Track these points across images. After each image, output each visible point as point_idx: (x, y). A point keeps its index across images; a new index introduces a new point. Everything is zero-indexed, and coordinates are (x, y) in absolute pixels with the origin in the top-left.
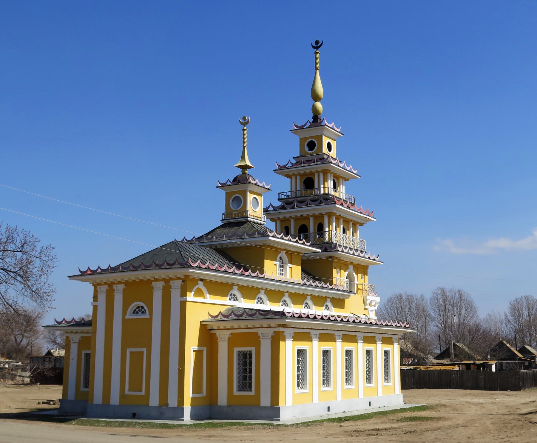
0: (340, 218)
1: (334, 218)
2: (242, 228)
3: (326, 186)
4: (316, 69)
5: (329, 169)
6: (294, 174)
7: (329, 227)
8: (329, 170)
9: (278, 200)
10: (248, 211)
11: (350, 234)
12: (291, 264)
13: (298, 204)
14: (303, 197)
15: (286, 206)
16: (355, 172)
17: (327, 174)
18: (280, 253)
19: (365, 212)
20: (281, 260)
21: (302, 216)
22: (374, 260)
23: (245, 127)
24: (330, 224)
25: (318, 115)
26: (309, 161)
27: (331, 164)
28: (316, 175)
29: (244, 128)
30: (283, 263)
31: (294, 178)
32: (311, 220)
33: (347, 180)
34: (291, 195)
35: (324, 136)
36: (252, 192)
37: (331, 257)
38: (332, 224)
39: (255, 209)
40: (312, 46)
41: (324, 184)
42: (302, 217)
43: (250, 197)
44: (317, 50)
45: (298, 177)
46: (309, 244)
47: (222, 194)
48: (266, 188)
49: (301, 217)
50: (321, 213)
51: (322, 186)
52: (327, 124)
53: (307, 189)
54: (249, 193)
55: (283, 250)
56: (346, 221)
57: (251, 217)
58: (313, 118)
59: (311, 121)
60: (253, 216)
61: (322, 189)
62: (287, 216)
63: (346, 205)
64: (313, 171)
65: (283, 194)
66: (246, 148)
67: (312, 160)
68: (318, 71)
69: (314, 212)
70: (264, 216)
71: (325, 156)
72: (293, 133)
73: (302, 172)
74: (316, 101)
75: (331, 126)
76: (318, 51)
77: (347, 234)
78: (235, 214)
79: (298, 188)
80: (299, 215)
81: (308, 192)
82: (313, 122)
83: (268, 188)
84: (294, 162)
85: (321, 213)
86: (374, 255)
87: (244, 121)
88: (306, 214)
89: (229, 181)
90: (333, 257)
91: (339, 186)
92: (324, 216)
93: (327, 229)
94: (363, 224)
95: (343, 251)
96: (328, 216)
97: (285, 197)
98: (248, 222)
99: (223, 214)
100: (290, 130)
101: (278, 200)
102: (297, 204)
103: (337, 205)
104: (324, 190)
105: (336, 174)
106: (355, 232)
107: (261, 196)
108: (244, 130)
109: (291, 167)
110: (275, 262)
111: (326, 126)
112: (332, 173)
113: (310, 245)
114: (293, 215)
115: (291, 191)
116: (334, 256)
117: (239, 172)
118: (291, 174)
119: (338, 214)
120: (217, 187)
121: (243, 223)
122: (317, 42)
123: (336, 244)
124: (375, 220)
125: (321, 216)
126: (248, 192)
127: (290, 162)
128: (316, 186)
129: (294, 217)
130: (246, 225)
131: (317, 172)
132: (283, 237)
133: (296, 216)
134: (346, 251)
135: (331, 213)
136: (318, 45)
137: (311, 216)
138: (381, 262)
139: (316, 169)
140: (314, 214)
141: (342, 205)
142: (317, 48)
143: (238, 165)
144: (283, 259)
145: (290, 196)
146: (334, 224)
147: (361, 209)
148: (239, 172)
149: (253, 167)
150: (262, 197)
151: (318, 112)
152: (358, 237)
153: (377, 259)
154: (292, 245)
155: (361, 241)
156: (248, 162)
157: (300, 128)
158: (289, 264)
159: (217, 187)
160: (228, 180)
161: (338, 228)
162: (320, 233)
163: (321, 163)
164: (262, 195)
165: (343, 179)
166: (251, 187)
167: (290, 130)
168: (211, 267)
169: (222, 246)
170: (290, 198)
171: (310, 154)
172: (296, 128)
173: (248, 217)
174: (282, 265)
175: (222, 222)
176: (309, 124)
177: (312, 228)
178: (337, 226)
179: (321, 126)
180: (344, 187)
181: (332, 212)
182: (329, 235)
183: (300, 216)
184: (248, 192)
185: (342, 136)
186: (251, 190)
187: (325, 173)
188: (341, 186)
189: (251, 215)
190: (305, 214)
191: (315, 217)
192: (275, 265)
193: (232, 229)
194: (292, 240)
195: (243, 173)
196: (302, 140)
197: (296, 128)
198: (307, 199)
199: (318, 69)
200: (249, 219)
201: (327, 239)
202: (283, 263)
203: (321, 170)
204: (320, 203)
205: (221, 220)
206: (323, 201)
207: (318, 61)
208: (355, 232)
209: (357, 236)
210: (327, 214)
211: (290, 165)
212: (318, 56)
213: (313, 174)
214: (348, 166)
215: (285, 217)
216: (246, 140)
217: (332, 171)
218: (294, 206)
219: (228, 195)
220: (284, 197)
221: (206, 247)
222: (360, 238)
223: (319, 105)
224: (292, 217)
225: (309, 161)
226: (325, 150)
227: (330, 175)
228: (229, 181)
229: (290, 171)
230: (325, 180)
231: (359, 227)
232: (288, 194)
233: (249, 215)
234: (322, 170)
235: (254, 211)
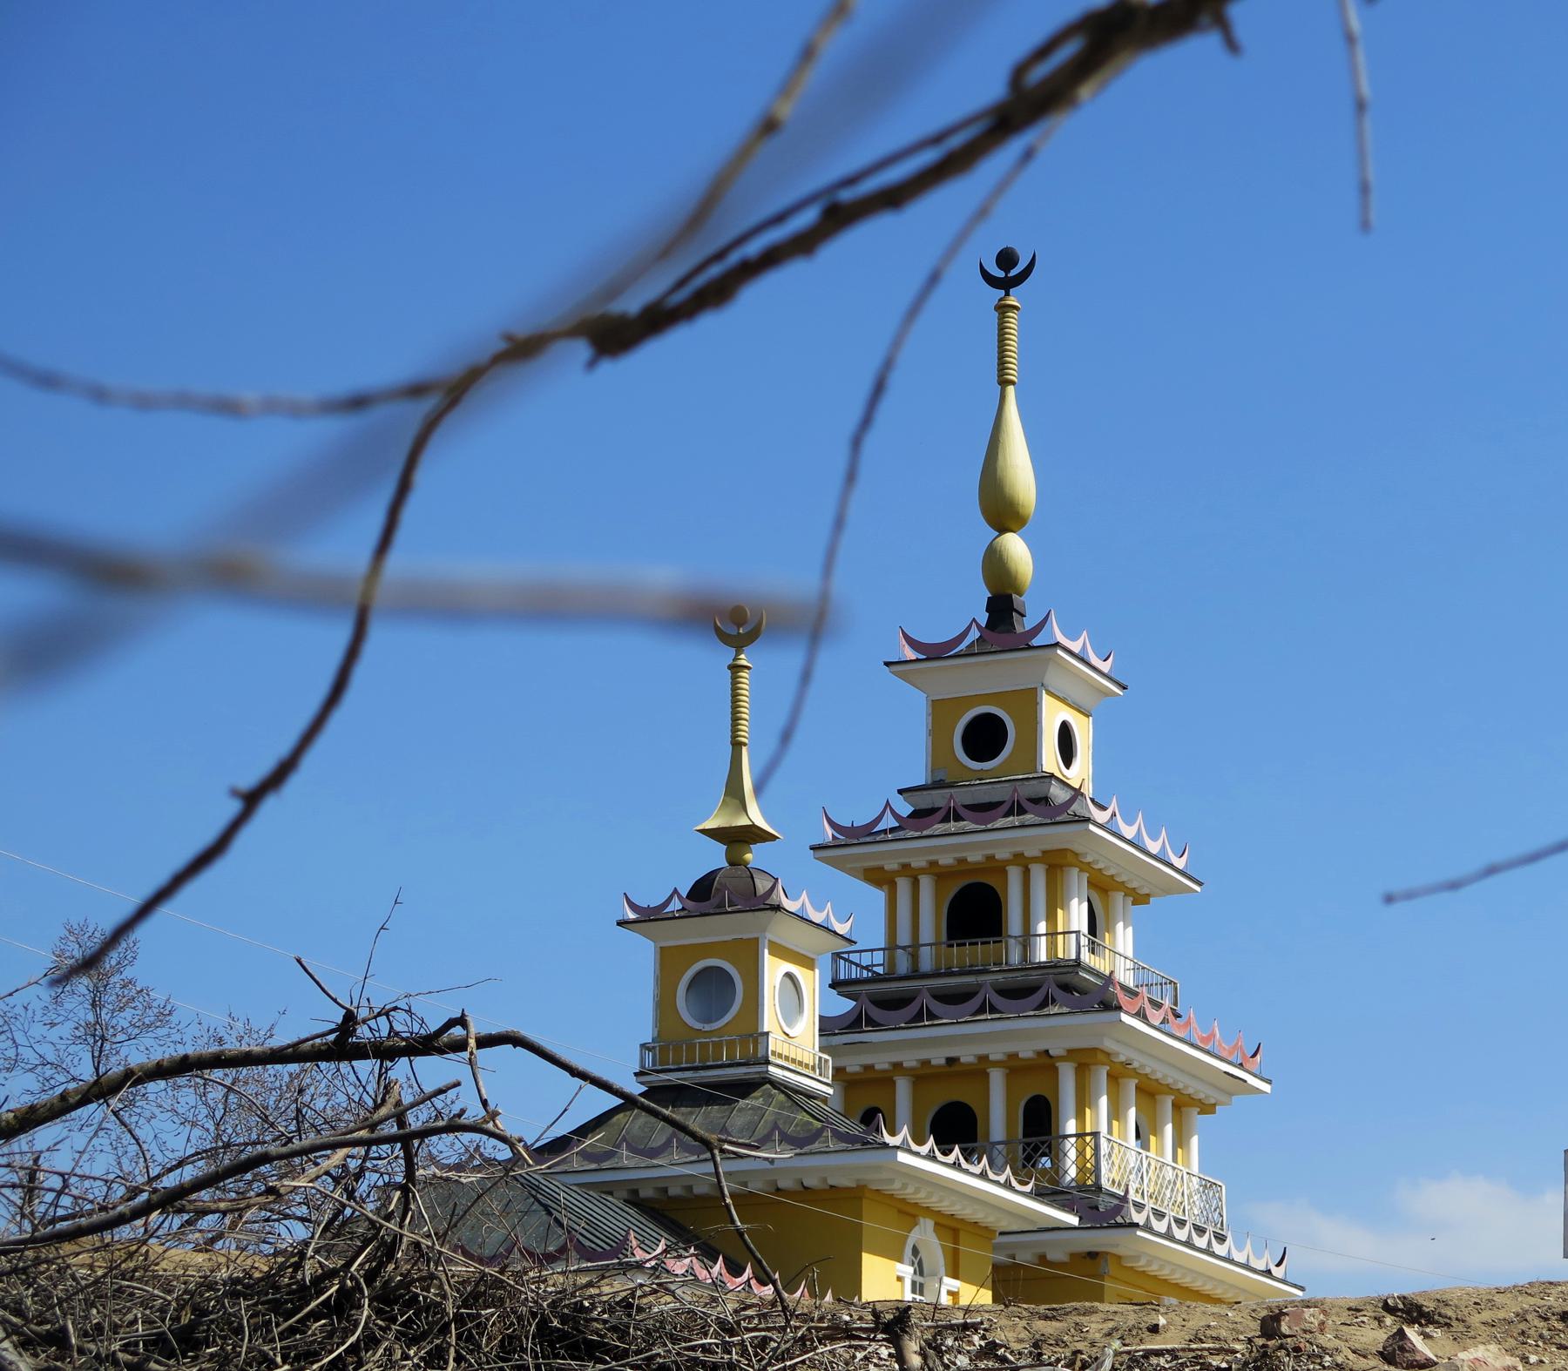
0: (1123, 1077)
1: (1103, 1072)
2: (740, 1110)
3: (1060, 929)
4: (1004, 383)
5: (1077, 848)
6: (906, 866)
7: (1080, 1116)
8: (1077, 854)
9: (830, 986)
10: (767, 1034)
11: (1161, 1152)
12: (955, 1276)
13: (937, 1007)
14: (952, 974)
15: (876, 1013)
16: (1180, 863)
17: (1062, 871)
18: (917, 1227)
19: (1231, 1053)
20: (916, 1257)
21: (951, 1061)
22: (1268, 1273)
23: (742, 656)
24: (1084, 1102)
25: (1014, 596)
26: (984, 809)
27: (1091, 827)
28: (1014, 874)
29: (736, 659)
30: (921, 1274)
31: (903, 885)
32: (997, 1079)
33: (1140, 899)
34: (891, 962)
35: (1050, 693)
36: (781, 952)
37: (1093, 1255)
38: (1094, 1105)
39: (789, 1024)
40: (985, 275)
41: (1051, 918)
42: (955, 1068)
43: (774, 970)
44: (1007, 294)
45: (926, 884)
46: (1028, 1188)
47: (641, 952)
48: (835, 933)
49: (948, 1069)
50: (1047, 1051)
51: (1042, 927)
52: (1061, 638)
53: (974, 940)
54: (770, 954)
55: (929, 1212)
56: (1149, 1092)
57: (779, 1062)
58: (987, 611)
59: (983, 618)
60: (787, 1058)
61: (1042, 943)
62: (882, 1062)
63: (1156, 1016)
64: (1002, 854)
65: (846, 956)
66: (744, 750)
67: (1000, 803)
68: (1011, 390)
69: (1011, 1047)
70: (826, 1061)
71: (1051, 790)
72: (903, 676)
73: (946, 860)
74: (1002, 530)
75: (1076, 647)
76: (1012, 301)
77: (1149, 1151)
78: (704, 1046)
79: (927, 933)
80: (938, 1057)
81: (974, 952)
82: (991, 625)
83: (841, 933)
84: (905, 809)
85: (1047, 1051)
86: (1267, 1255)
87: (739, 626)
88: (918, 1058)
89: (676, 897)
90: (1107, 1253)
91: (1110, 928)
92: (1057, 1064)
93: (1071, 1127)
94: (1214, 1105)
95: (1148, 1228)
96: (1074, 1065)
97: (865, 974)
98: (768, 1086)
99: (643, 1046)
100: (887, 664)
101: (830, 986)
102: (869, 1013)
103: (1125, 1018)
104: (1052, 946)
105: (1112, 876)
106: (1180, 1141)
107: (813, 970)
108: (735, 668)
109: (901, 834)
110: (898, 1265)
111: (1059, 652)
112: (1085, 867)
113: (1031, 1193)
114: (910, 1059)
115: (891, 947)
116: (1103, 1250)
117: (715, 857)
118: (891, 865)
119: (1122, 1058)
120: (620, 924)
121: (745, 1088)
122: (1006, 258)
123: (1124, 1199)
124: (1266, 1087)
125: (1046, 1064)
126: (766, 951)
127: (891, 808)
128: (1014, 924)
129: (912, 1069)
130: (757, 1098)
131: (1022, 861)
132: (934, 1151)
133: (926, 1063)
134: (1160, 1226)
135: (1094, 1051)
136: (1013, 273)
137: (997, 1064)
138: (1295, 1286)
139: (1018, 849)
140: (1013, 1056)
141: (1141, 1015)
142: (1006, 285)
143: (701, 827)
144: (923, 1254)
145: (880, 970)
146: (1103, 1101)
147: (1214, 1035)
148: (715, 857)
149: (774, 838)
150: (817, 971)
151: (1016, 578)
152: (1195, 1169)
153: (1278, 1272)
154: (962, 1190)
155: (1207, 1186)
156: (755, 815)
157: (933, 653)
158: (947, 1276)
159: (620, 924)
160: (675, 891)
161: (1115, 1123)
162: (1043, 1143)
163: (1038, 820)
164: (817, 963)
165: (1126, 895)
166: (780, 930)
167: (887, 664)
168: (700, 1274)
169: (665, 1190)
170: (877, 979)
171: (980, 775)
172: (910, 654)
173: (768, 1062)
174: (919, 1279)
175: (642, 1083)
176: (974, 634)
177: (999, 1119)
178: (1116, 1113)
179: (1031, 648)
180: (1130, 929)
181: (1100, 1047)
182: (1081, 1153)
183: (943, 1061)
184: (766, 951)
185: (1121, 693)
186: (778, 941)
187: (1057, 863)
188: (1120, 926)
189: (780, 1056)
190: (967, 1055)
191: (1015, 1068)
192: (900, 1279)
193: (691, 1113)
194: (991, 1175)
195: (732, 864)
196: (941, 710)
197: (910, 654)
198: (980, 986)
199: (1012, 383)
200: (771, 1068)
201: (1072, 1172)
202: (921, 1274)
203: (1011, 857)
204: (1044, 1004)
205: (636, 1074)
206: (1058, 994)
207: (1013, 345)
208: (1180, 1141)
209: (1187, 1163)
210: (1072, 1054)
211: (889, 822)
212: (1013, 320)
213: (1000, 869)
214: (1154, 838)
215: (868, 1068)
216: (745, 712)
217: (1089, 859)
218: (918, 1017)
219: (669, 961)
220: (861, 973)
221: (588, 1190)
222: (1199, 1172)
223: (1016, 547)
224: (906, 1069)
225: (984, 809)
226: (1050, 759)
227: (1078, 876)
228: (676, 897)
229: (888, 855)
230: (1055, 902)
231: (1198, 1120)
232: (866, 959)
233: (774, 1053)
234: (1044, 852)
235: (785, 1033)
